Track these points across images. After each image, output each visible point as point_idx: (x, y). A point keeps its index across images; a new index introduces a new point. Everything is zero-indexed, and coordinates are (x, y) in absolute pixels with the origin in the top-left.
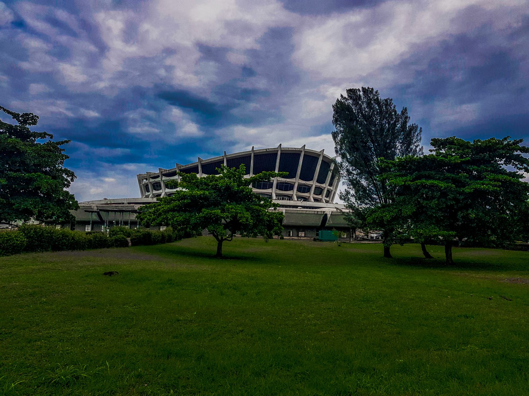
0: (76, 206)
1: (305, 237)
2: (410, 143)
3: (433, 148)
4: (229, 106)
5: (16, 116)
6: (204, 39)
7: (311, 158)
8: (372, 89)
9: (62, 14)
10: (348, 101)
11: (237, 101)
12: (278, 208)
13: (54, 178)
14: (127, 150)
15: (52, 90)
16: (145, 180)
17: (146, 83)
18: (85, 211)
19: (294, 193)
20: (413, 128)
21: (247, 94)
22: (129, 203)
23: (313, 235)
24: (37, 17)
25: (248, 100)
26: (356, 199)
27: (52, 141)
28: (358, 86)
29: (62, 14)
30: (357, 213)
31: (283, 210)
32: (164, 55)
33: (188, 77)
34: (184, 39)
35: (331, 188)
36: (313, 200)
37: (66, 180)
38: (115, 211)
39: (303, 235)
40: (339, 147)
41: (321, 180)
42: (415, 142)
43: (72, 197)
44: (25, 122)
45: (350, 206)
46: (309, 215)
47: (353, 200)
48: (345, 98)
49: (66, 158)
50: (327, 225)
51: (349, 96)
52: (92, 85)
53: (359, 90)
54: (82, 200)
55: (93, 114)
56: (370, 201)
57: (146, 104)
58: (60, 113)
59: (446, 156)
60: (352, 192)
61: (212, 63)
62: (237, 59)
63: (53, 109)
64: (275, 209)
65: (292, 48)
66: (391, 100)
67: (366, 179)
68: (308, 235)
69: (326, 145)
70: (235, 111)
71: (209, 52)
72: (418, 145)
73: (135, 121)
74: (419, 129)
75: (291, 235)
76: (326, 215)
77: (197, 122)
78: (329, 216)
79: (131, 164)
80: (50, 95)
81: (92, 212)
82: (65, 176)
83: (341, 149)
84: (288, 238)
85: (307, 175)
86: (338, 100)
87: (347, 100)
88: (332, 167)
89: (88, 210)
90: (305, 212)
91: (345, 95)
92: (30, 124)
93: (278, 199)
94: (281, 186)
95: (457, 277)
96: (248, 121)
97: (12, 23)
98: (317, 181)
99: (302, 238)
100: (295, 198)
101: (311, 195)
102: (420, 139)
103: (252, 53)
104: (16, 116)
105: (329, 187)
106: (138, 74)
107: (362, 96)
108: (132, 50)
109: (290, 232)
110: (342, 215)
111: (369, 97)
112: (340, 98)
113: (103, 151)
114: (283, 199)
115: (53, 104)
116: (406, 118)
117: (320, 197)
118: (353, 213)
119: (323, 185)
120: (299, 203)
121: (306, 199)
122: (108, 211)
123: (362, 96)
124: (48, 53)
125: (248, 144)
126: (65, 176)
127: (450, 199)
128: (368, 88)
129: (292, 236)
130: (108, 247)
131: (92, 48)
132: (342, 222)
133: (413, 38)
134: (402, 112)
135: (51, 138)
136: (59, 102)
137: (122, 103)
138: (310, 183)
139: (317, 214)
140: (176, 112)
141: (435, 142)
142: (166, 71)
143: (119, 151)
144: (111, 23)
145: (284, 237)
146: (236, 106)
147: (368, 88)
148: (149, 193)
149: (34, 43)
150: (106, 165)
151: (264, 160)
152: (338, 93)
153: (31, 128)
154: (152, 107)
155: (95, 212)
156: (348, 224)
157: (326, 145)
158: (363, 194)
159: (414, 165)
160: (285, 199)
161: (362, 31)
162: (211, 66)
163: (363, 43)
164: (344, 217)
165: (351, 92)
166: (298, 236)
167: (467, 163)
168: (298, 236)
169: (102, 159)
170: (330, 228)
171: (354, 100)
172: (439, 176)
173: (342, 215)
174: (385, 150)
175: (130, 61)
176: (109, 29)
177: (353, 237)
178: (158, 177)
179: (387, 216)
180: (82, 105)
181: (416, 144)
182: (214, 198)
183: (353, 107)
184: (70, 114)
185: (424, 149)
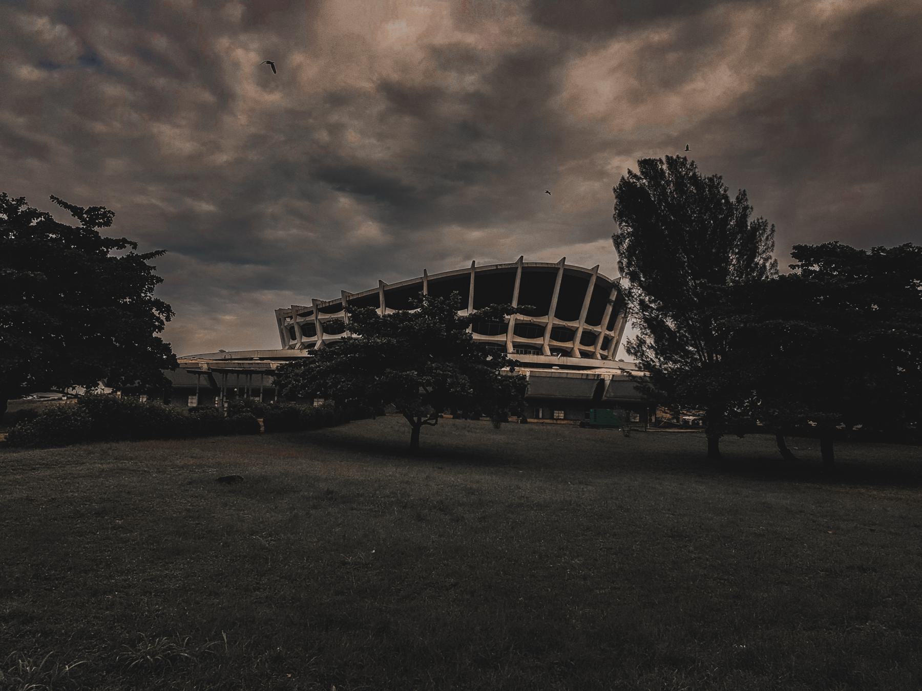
0: (172, 362)
2: (754, 253)
5: (77, 212)
6: (395, 77)
8: (685, 159)
12: (517, 369)
16: (288, 320)
20: (759, 226)
21: (468, 171)
22: (261, 359)
27: (135, 252)
28: (660, 154)
33: (363, 141)
34: (358, 79)
35: (612, 334)
37: (158, 319)
38: (238, 372)
39: (562, 416)
41: (594, 318)
43: (166, 348)
44: (92, 222)
45: (647, 366)
47: (651, 354)
48: (635, 176)
49: (157, 282)
51: (642, 173)
53: (661, 161)
54: (184, 354)
60: (650, 341)
61: (407, 119)
63: (140, 199)
64: (512, 370)
66: (721, 178)
69: (602, 258)
71: (404, 99)
72: (770, 257)
74: (769, 228)
76: (603, 380)
78: (608, 382)
79: (266, 291)
85: (568, 311)
89: (194, 371)
91: (636, 170)
92: (100, 225)
94: (521, 329)
96: (470, 216)
98: (588, 321)
99: (559, 422)
100: (547, 350)
101: (577, 346)
102: (773, 245)
103: (475, 99)
104: (77, 212)
105: (608, 332)
108: (274, 98)
110: (631, 381)
113: (222, 269)
117: (591, 349)
119: (598, 329)
121: (567, 353)
129: (543, 418)
131: (207, 97)
133: (760, 69)
138: (543, 320)
141: (801, 253)
144: (239, 53)
148: (295, 342)
149: (112, 90)
151: (494, 284)
153: (103, 232)
157: (602, 258)
158: (667, 344)
161: (672, 57)
164: (636, 384)
166: (552, 418)
168: (552, 418)
173: (631, 381)
176: (236, 65)
185: (778, 262)
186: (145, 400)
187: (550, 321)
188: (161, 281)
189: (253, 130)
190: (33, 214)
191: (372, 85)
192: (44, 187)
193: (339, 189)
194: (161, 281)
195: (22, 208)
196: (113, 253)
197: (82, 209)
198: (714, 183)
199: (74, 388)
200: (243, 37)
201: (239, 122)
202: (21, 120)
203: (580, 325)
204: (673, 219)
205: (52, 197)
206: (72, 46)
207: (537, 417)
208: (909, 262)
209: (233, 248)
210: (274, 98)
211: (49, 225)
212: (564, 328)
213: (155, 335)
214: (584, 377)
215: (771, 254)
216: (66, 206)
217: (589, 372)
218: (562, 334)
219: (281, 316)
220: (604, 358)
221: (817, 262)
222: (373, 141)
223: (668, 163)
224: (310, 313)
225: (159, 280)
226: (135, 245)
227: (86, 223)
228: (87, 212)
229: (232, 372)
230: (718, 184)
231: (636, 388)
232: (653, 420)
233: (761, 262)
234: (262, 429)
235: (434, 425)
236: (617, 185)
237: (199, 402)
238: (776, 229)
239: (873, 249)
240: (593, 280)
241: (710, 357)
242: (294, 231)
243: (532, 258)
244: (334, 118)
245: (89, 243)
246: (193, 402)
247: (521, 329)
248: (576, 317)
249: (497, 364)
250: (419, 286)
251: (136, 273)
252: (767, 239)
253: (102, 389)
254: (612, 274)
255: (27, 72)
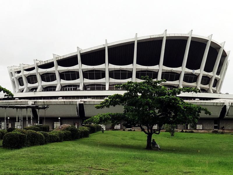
23: (211, 127)
35: (219, 77)
41: (209, 68)
50: (226, 117)
75: (189, 128)
76: (225, 106)
78: (228, 107)
85: (194, 64)
95: (224, 135)
99: (199, 131)
105: (217, 76)
117: (206, 87)
119: (210, 74)
138: (196, 72)
139: (216, 105)
166: (196, 129)
178: (33, 69)
187: (183, 70)
203: (201, 72)
212: (192, 74)
214: (215, 104)
220: (215, 92)
224: (33, 69)
235: (158, 134)
248: (198, 67)
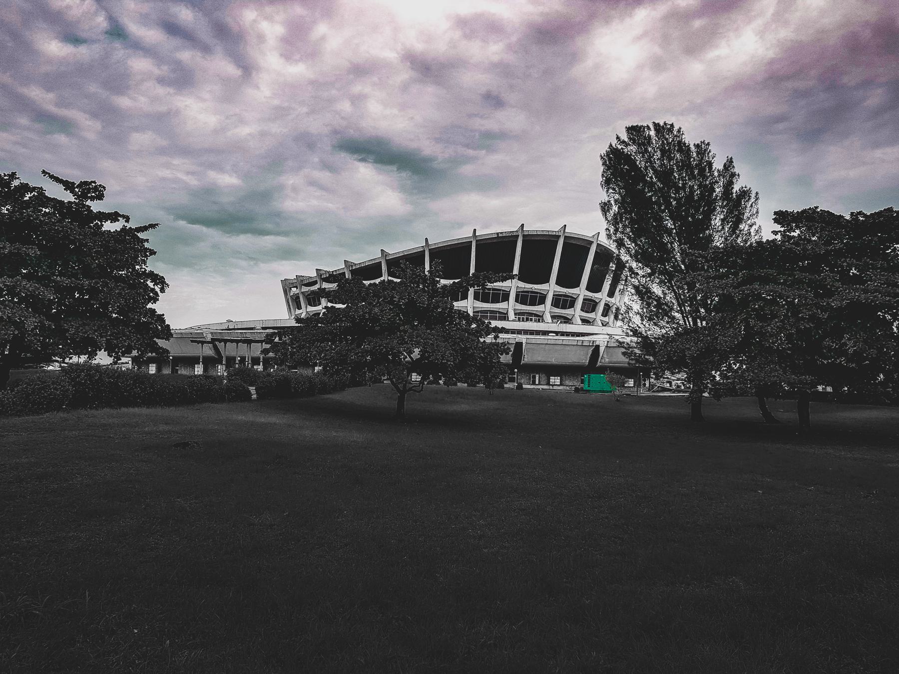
0: (166, 333)
1: (561, 384)
2: (739, 220)
3: (778, 228)
4: (457, 161)
5: (69, 186)
6: (419, 47)
7: (576, 248)
8: (672, 125)
9: (185, 15)
10: (630, 148)
11: (471, 152)
12: (501, 335)
13: (132, 287)
14: (281, 240)
15: (164, 143)
16: (294, 289)
17: (316, 125)
18: (192, 341)
19: (547, 309)
20: (744, 194)
21: (490, 140)
22: (264, 328)
24: (144, 19)
25: (490, 149)
26: (642, 320)
27: (128, 226)
28: (644, 121)
29: (185, 15)
30: (646, 343)
31: (522, 338)
32: (351, 76)
33: (386, 114)
34: (382, 49)
36: (580, 322)
37: (153, 290)
38: (237, 342)
39: (558, 381)
40: (612, 229)
41: (595, 286)
42: (749, 218)
43: (161, 318)
44: (83, 196)
45: (636, 333)
46: (568, 348)
47: (637, 320)
48: (624, 142)
49: (151, 254)
51: (630, 139)
52: (229, 134)
53: (648, 128)
54: (177, 322)
55: (227, 180)
56: (668, 322)
57: (316, 160)
58: (176, 180)
59: (799, 241)
60: (636, 307)
61: (431, 89)
62: (473, 80)
63: (166, 173)
64: (496, 337)
65: (574, 58)
66: (708, 144)
67: (661, 283)
68: (567, 382)
69: (591, 223)
70: (467, 169)
71: (427, 69)
72: (754, 224)
73: (295, 189)
74: (753, 195)
75: (537, 382)
77: (403, 189)
78: (602, 349)
79: (284, 262)
80: (162, 151)
81: (203, 343)
82: (150, 284)
83: (616, 230)
84: (532, 387)
85: (569, 278)
86: (611, 145)
87: (627, 145)
88: (613, 266)
89: (195, 338)
90: (560, 342)
91: (624, 137)
92: (92, 199)
93: (519, 320)
94: (522, 298)
96: (487, 184)
97: (106, 33)
98: (588, 289)
99: (555, 387)
100: (548, 317)
101: (577, 312)
102: (757, 212)
103: (503, 69)
104: (69, 186)
105: (608, 299)
106: (305, 110)
107: (654, 139)
108: (298, 70)
109: (534, 377)
110: (618, 347)
111: (667, 139)
112: (614, 142)
113: (243, 241)
114: (527, 319)
115: (167, 166)
116: (733, 175)
117: (591, 315)
118: (637, 343)
120: (555, 327)
121: (567, 320)
122: (226, 341)
123: (654, 139)
124: (161, 81)
125: (460, 225)
126: (150, 284)
127: (803, 319)
128: (665, 124)
129: (539, 384)
130: (214, 401)
131: (231, 69)
132: (619, 358)
133: (785, 34)
134: (725, 165)
135: (127, 221)
136: (176, 161)
137: (275, 161)
140: (365, 173)
141: (781, 217)
142: (353, 103)
143: (268, 241)
144: (265, 26)
145: (524, 386)
146: (468, 160)
147: (665, 124)
148: (300, 311)
149: (140, 64)
150: (243, 263)
151: (495, 253)
152: (614, 132)
153: (95, 206)
154: (327, 166)
155: (208, 342)
156: (629, 364)
157: (591, 223)
158: (657, 310)
159: (741, 259)
160: (531, 320)
161: (697, 23)
162: (430, 92)
163: (695, 46)
164: (624, 350)
165: (631, 130)
166: (548, 384)
167: (839, 253)
168: (548, 384)
169: (236, 253)
170: (603, 370)
171: (639, 145)
172: (785, 277)
173: (618, 347)
174: (695, 233)
175: (290, 89)
176: (261, 38)
177: (645, 385)
178: (315, 283)
179: (693, 349)
180: (212, 166)
181: (749, 222)
182: (389, 319)
183: (638, 158)
184: (193, 181)
185: (763, 227)
186: (154, 369)
187: (551, 288)
188: (155, 253)
189: (276, 102)
190: (25, 188)
191: (396, 55)
192: (42, 164)
193: (363, 160)
194: (155, 253)
195: (16, 183)
196: (108, 226)
197: (73, 184)
198: (703, 149)
199: (71, 358)
200: (268, 9)
201: (262, 92)
202: (51, 96)
204: (659, 183)
205: (44, 172)
206: (101, 21)
207: (534, 383)
208: (888, 225)
209: (240, 219)
210: (298, 70)
211: (42, 198)
213: (150, 306)
215: (756, 220)
216: (57, 180)
217: (586, 338)
218: (564, 302)
219: (287, 286)
221: (797, 227)
222: (395, 111)
223: (656, 130)
225: (153, 253)
226: (127, 219)
227: (78, 197)
228: (79, 186)
229: (232, 341)
230: (705, 150)
231: (624, 354)
232: (647, 385)
233: (746, 229)
234: (254, 396)
236: (603, 152)
237: (205, 370)
238: (760, 196)
239: (852, 214)
240: (593, 249)
241: (695, 323)
242: (314, 202)
243: (535, 226)
244: (357, 89)
245: (78, 215)
246: (199, 370)
247: (522, 298)
249: (479, 333)
250: (422, 253)
251: (131, 245)
252: (751, 206)
253: (103, 359)
254: (603, 240)
255: (54, 48)
